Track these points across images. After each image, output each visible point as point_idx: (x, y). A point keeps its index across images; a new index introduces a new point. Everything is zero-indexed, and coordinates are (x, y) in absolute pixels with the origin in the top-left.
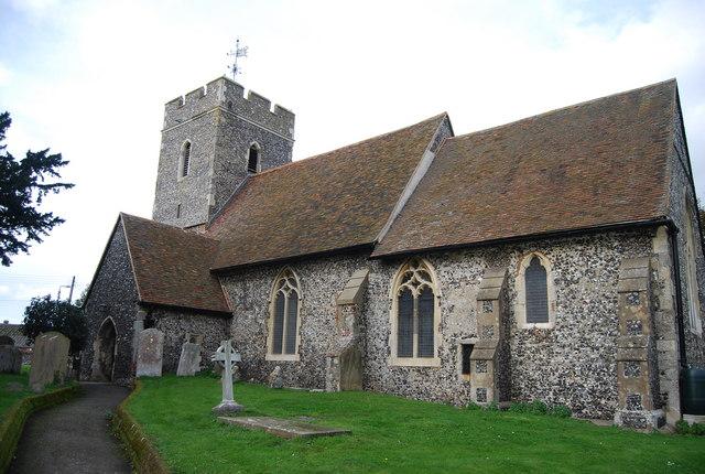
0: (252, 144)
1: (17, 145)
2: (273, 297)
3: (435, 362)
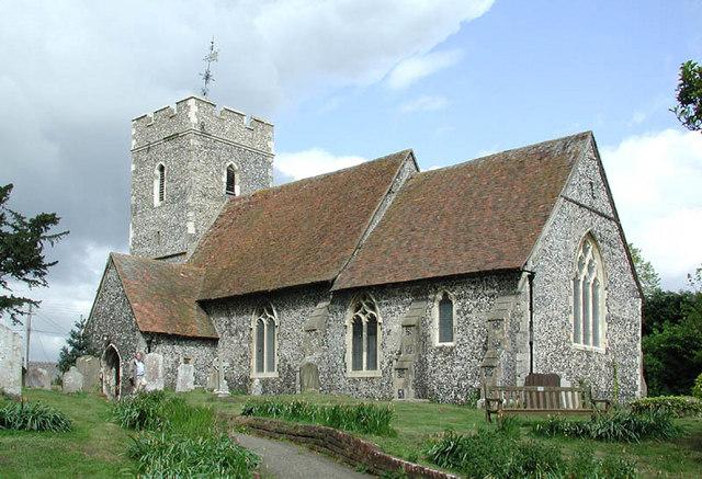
0: (228, 164)
1: (24, 205)
2: (254, 325)
3: (378, 373)
